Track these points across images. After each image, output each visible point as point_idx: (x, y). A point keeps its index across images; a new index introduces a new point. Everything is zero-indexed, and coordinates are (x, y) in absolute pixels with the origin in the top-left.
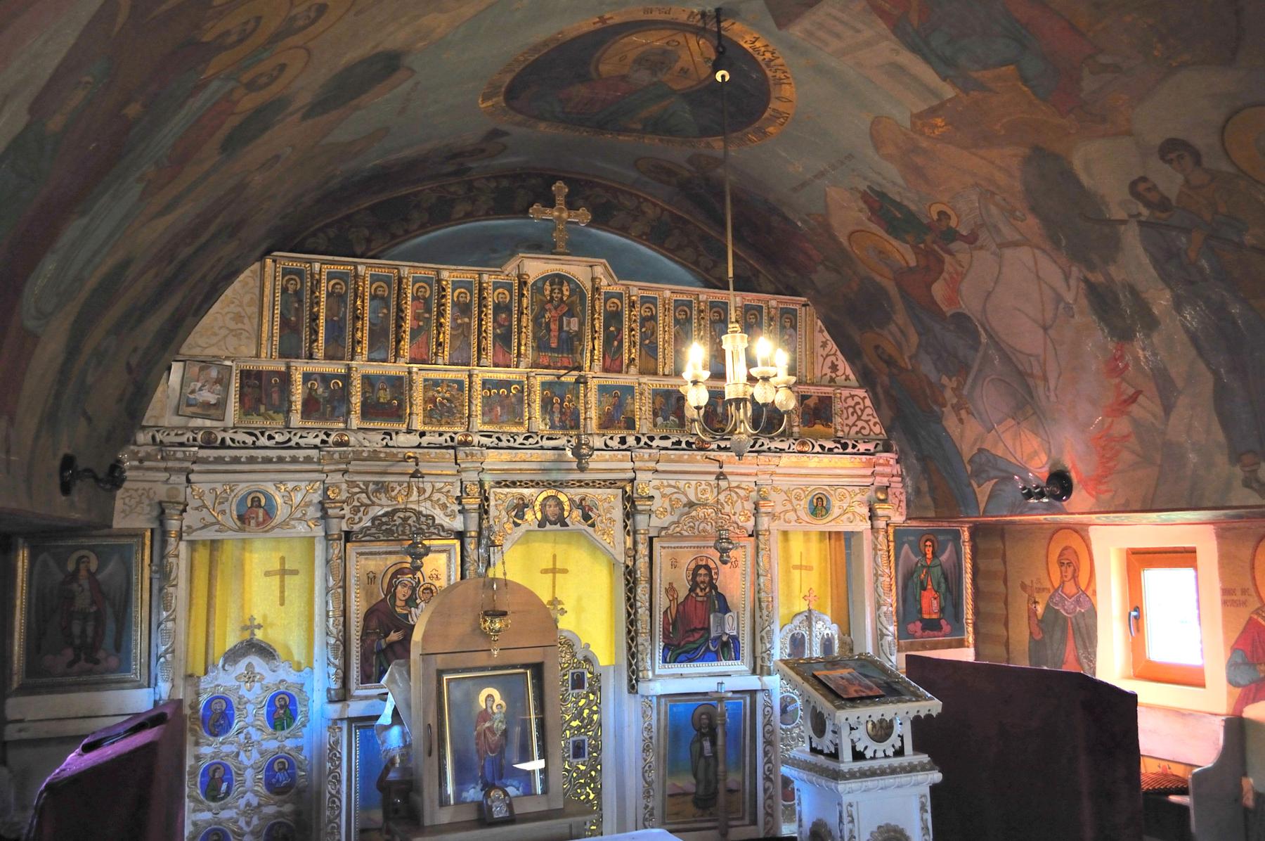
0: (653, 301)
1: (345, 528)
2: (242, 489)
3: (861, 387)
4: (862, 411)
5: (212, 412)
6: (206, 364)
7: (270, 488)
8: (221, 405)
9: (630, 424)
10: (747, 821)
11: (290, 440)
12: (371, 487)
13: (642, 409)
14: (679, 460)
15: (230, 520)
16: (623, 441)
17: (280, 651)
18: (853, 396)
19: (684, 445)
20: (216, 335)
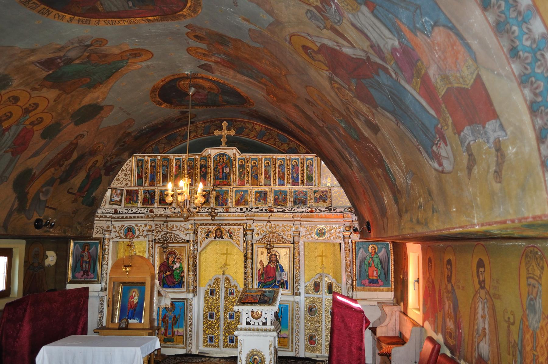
0: (256, 160)
1: (154, 238)
6: (116, 189)
8: (121, 201)
9: (246, 203)
10: (290, 350)
13: (251, 198)
14: (262, 216)
16: (241, 209)
19: (264, 211)
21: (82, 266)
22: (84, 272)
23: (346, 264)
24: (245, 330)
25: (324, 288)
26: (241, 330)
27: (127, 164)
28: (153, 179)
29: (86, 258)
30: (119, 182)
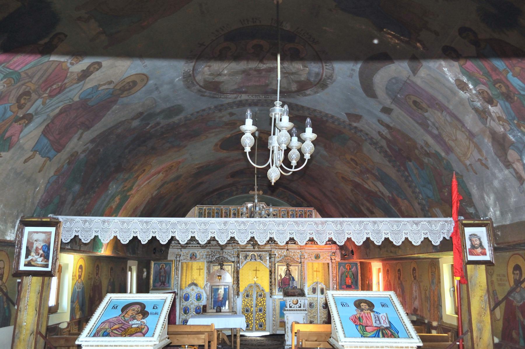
2: (191, 252)
7: (196, 252)
15: (189, 258)
17: (199, 285)
21: (160, 279)
22: (162, 283)
23: (333, 276)
24: (290, 310)
25: (319, 291)
26: (288, 310)
29: (162, 274)
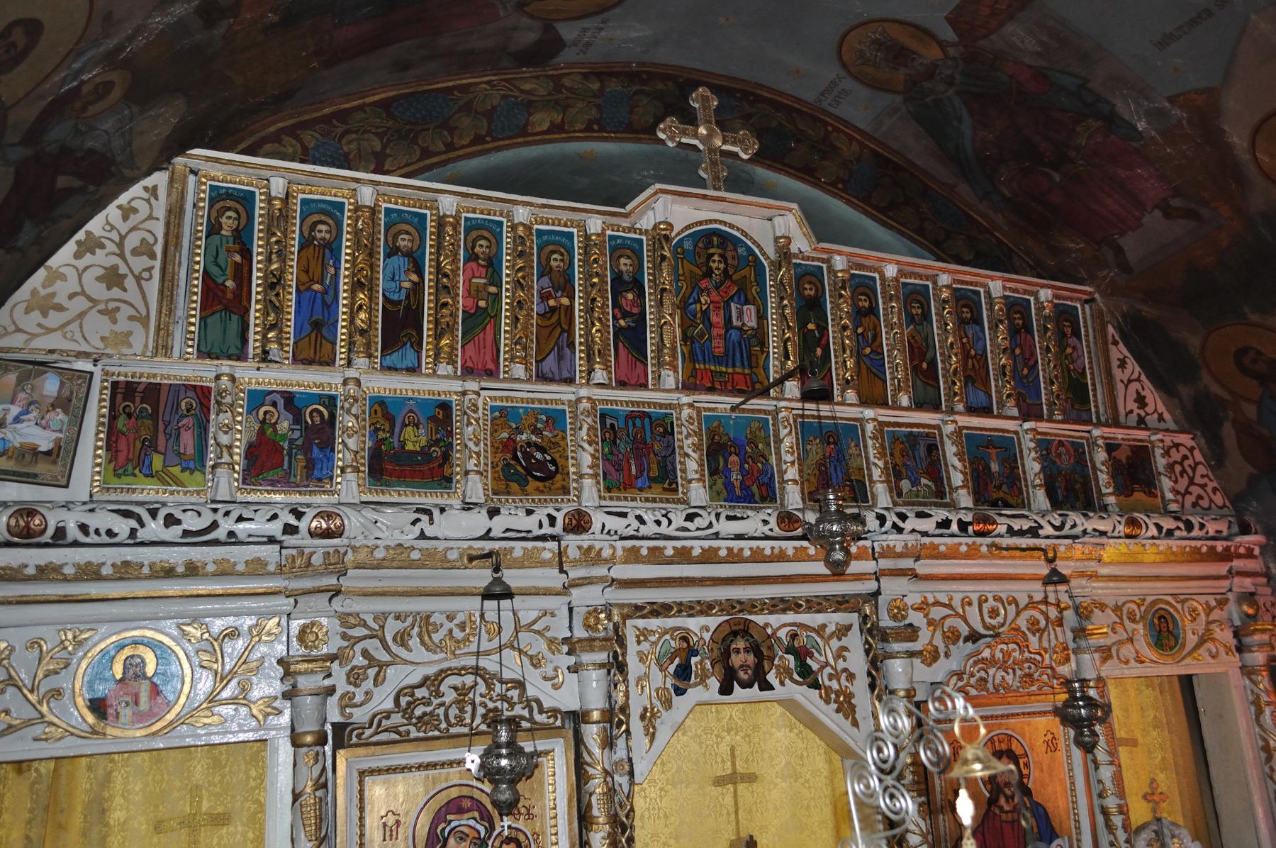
1: (334, 716)
3: (1182, 432)
4: (1194, 469)
5: (41, 468)
8: (62, 455)
11: (214, 525)
12: (392, 627)
18: (1177, 446)
19: (954, 527)
20: (59, 308)
27: (127, 212)
28: (317, 325)
30: (55, 319)
